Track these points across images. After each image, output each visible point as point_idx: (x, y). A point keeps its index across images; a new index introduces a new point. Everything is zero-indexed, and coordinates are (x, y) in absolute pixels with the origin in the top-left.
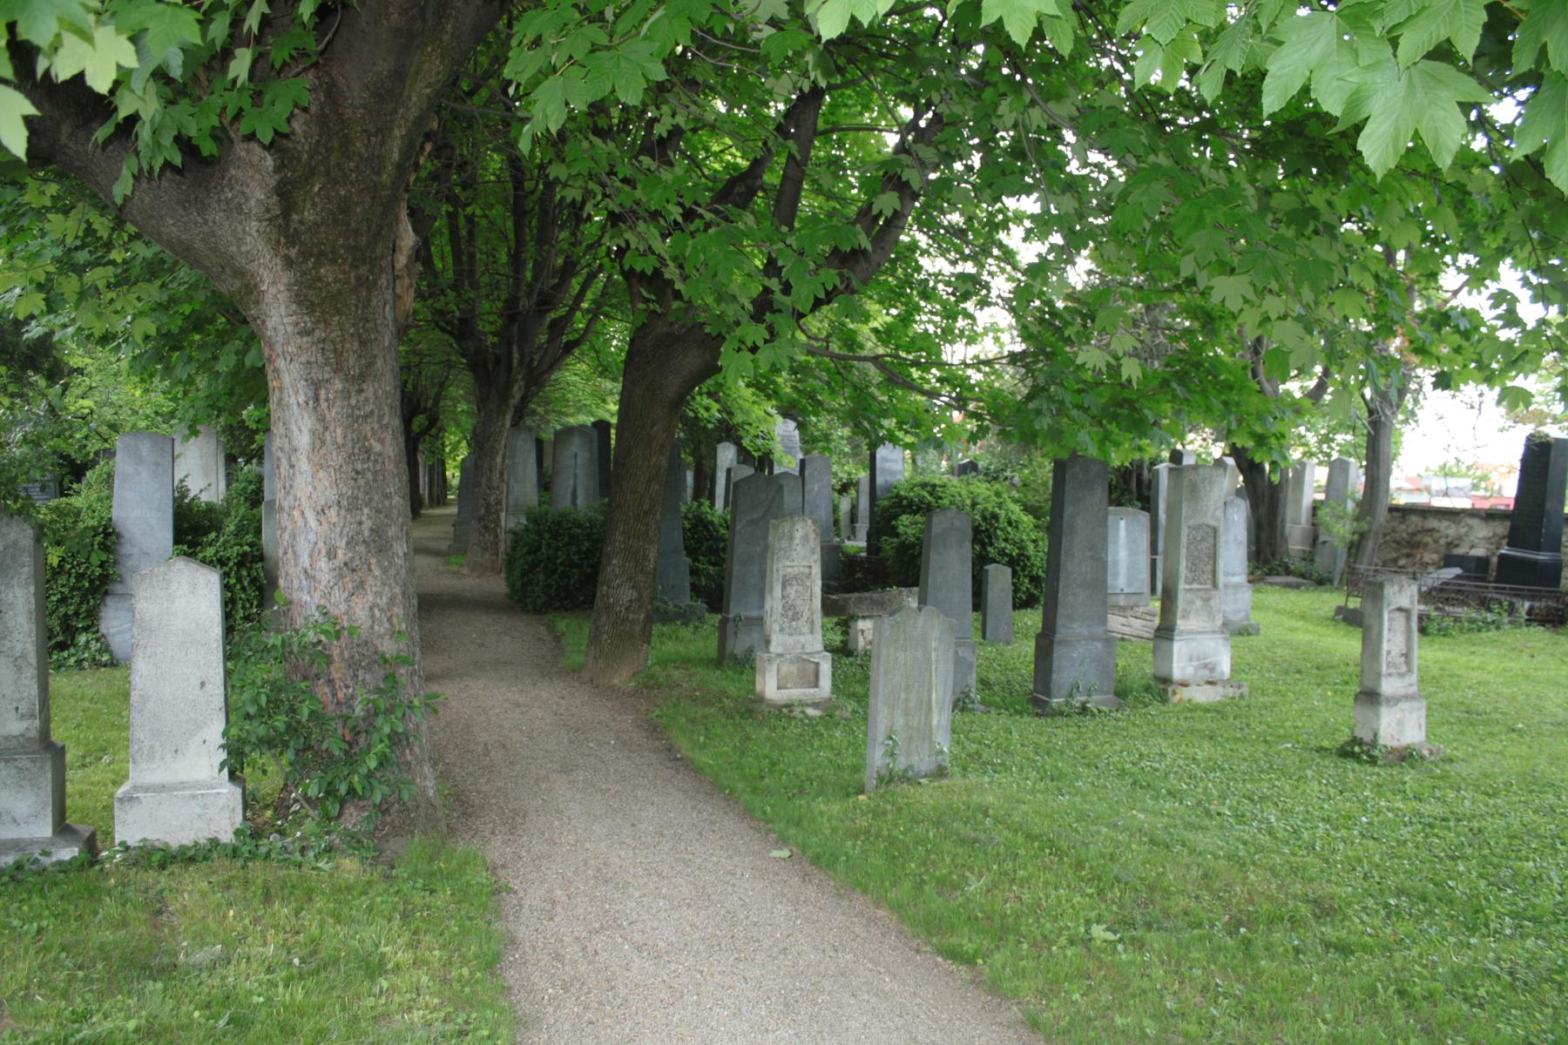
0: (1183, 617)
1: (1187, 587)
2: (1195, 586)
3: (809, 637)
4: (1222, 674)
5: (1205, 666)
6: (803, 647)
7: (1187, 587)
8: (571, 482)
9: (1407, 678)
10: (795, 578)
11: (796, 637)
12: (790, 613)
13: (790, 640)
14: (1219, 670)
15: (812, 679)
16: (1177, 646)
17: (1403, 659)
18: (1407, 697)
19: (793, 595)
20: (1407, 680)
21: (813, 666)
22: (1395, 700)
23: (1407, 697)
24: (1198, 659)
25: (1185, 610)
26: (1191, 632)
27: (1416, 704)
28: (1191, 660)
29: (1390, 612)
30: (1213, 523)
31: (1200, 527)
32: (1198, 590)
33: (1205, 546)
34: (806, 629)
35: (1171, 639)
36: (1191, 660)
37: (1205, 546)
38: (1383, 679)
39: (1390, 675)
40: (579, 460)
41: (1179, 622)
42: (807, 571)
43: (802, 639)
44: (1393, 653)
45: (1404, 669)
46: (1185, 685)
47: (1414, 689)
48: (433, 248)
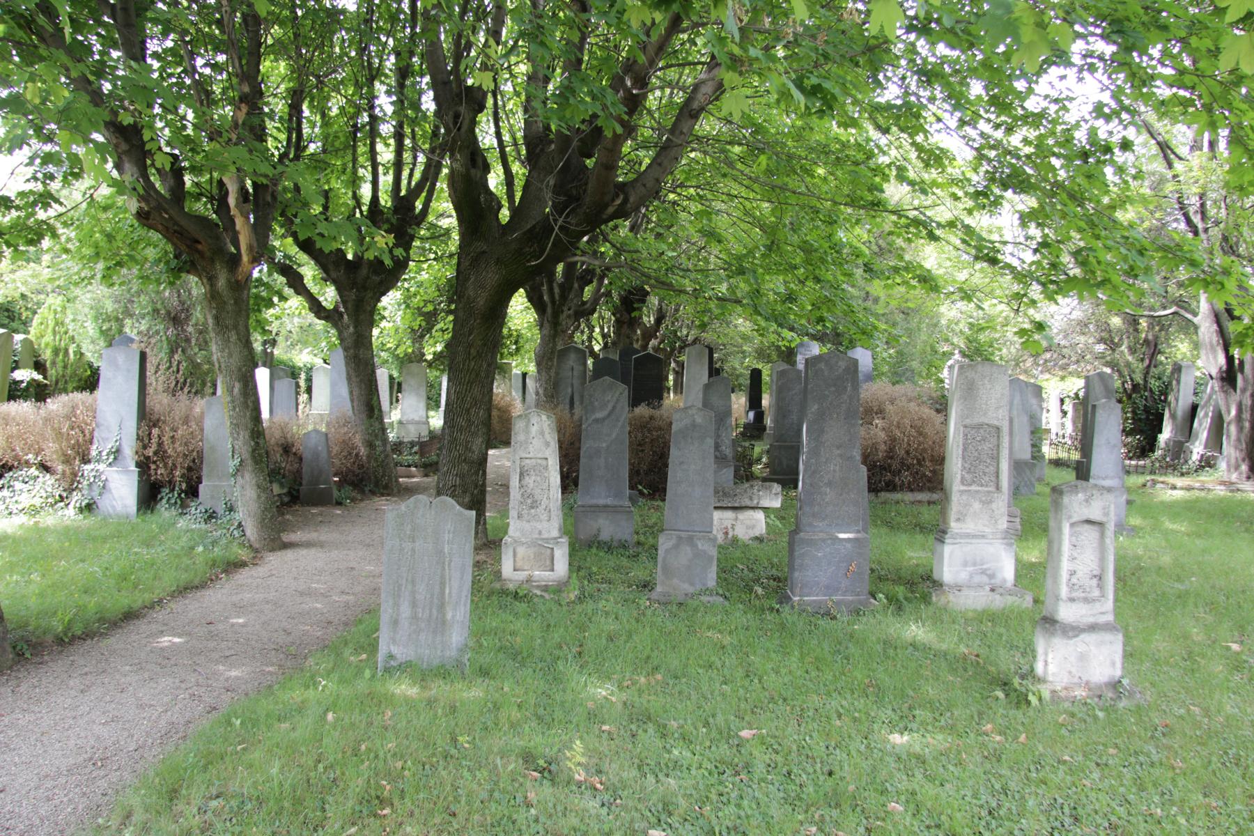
0: (958, 520)
1: (963, 488)
2: (974, 488)
3: (545, 524)
4: (1005, 581)
5: (983, 572)
6: (540, 533)
7: (963, 488)
8: (569, 390)
9: (1097, 605)
10: (534, 468)
11: (533, 524)
12: (529, 501)
13: (527, 526)
14: (999, 576)
15: (548, 563)
16: (947, 549)
17: (1095, 582)
18: (1093, 628)
19: (531, 485)
20: (1098, 607)
21: (549, 551)
22: (1071, 631)
23: (1093, 628)
24: (974, 564)
25: (959, 512)
26: (968, 536)
27: (1108, 637)
28: (965, 564)
29: (1072, 525)
30: (996, 423)
31: (979, 427)
32: (977, 492)
33: (986, 446)
34: (544, 517)
35: (941, 541)
36: (965, 564)
37: (986, 446)
38: (1061, 603)
39: (1072, 600)
40: (575, 373)
41: (953, 524)
42: (544, 462)
43: (539, 526)
44: (1079, 574)
45: (1096, 593)
46: (959, 588)
47: (1110, 618)
48: (152, 178)
